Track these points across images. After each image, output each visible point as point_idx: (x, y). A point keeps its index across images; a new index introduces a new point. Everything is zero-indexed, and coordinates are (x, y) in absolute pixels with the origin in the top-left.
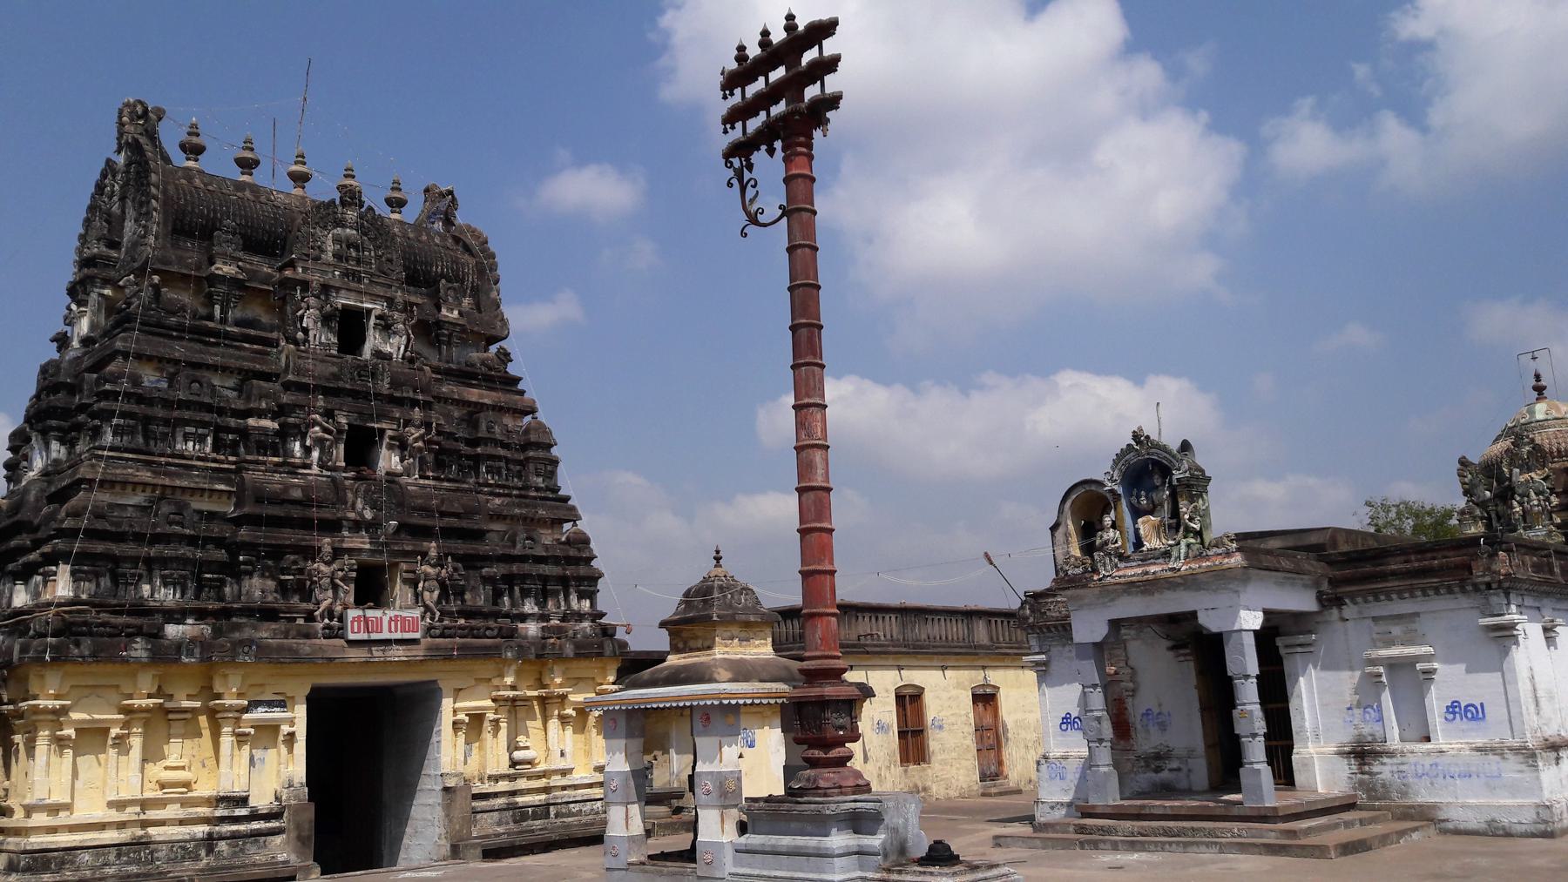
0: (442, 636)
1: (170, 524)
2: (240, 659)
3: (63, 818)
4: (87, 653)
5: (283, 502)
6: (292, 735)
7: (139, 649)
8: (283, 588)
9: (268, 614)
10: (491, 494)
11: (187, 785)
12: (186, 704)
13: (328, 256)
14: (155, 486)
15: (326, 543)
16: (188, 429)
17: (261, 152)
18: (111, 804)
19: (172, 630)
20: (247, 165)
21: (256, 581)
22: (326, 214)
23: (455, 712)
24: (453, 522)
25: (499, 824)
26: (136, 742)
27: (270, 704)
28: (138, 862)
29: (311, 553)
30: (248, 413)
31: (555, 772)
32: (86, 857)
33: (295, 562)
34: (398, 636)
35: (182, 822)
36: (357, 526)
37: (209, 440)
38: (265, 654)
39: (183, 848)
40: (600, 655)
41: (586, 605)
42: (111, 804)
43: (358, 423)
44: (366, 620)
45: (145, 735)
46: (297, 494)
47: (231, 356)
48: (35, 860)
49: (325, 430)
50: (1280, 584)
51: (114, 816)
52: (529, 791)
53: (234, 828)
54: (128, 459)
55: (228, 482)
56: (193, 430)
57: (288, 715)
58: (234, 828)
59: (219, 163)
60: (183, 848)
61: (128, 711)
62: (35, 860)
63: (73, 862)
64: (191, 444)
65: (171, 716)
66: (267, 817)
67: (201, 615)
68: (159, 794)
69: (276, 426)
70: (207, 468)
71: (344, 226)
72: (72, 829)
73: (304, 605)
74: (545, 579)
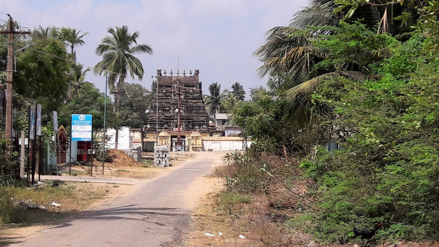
15: (172, 121)
20: (191, 74)
29: (171, 122)
36: (176, 119)
59: (168, 75)
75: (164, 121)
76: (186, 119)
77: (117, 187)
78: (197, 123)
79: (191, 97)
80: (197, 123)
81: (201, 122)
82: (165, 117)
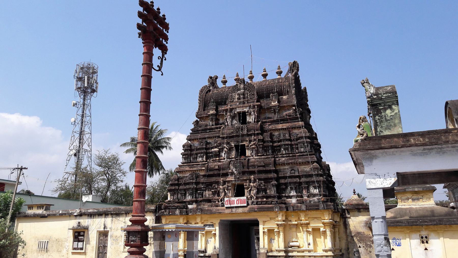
6: (215, 234)
7: (178, 212)
8: (214, 194)
9: (209, 201)
10: (282, 157)
13: (236, 100)
15: (221, 180)
18: (324, 250)
19: (190, 207)
20: (279, 73)
22: (235, 88)
23: (263, 228)
24: (261, 168)
27: (209, 225)
29: (218, 183)
31: (306, 250)
33: (214, 186)
34: (239, 205)
42: (324, 250)
46: (217, 167)
49: (227, 148)
50: (422, 154)
57: (214, 228)
59: (258, 79)
64: (200, 159)
67: (196, 202)
69: (218, 150)
71: (240, 90)
74: (300, 183)
76: (260, 172)
78: (289, 180)
79: (276, 117)
80: (289, 180)
81: (303, 180)
82: (208, 169)
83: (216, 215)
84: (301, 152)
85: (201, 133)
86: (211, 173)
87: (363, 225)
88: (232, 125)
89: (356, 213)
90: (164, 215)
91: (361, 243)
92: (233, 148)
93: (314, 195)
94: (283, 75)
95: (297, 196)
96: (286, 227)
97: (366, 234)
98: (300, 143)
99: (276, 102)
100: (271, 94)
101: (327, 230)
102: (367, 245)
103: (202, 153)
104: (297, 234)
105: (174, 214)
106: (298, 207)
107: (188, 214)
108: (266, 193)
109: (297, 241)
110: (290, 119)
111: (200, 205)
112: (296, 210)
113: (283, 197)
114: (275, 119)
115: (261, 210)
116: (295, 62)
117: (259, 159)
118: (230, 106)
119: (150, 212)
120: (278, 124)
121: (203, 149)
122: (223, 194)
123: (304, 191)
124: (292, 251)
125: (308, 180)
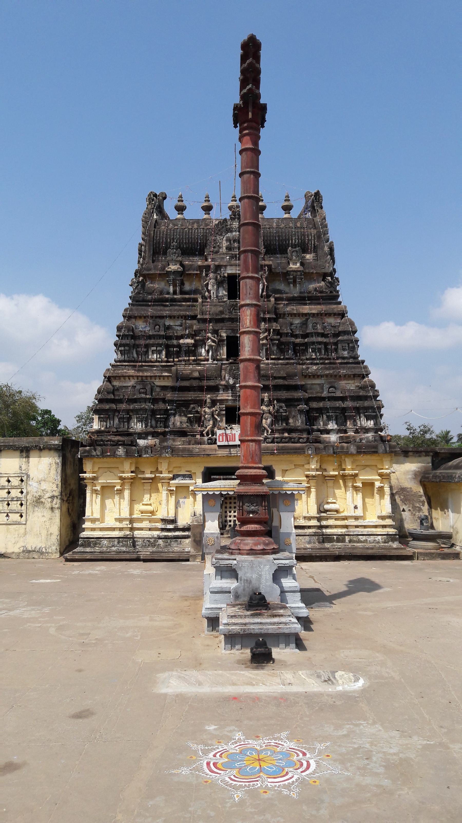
0: (273, 442)
1: (140, 393)
2: (164, 455)
3: (98, 525)
4: (99, 454)
5: (191, 379)
7: (121, 451)
8: (190, 421)
9: (182, 433)
10: (311, 364)
11: (152, 513)
12: (332, 473)
13: (224, 250)
14: (138, 377)
15: (208, 397)
16: (153, 348)
17: (213, 202)
18: (379, 517)
19: (141, 442)
20: (287, 209)
21: (177, 418)
22: (223, 226)
24: (281, 382)
25: (309, 543)
26: (127, 493)
27: (184, 476)
28: (126, 546)
29: (202, 403)
30: (182, 337)
31: (351, 517)
32: (105, 542)
33: (194, 408)
35: (150, 529)
36: (227, 388)
37: (164, 353)
38: (174, 452)
39: (149, 541)
40: (376, 452)
41: (371, 424)
42: (379, 517)
43: (232, 335)
44: (226, 435)
45: (131, 490)
46: (196, 374)
47: (175, 310)
48: (85, 542)
49: (214, 341)
51: (118, 525)
52: (336, 527)
53: (166, 534)
54: (125, 366)
55: (170, 371)
56: (155, 348)
58: (166, 534)
59: (194, 213)
60: (149, 541)
61: (121, 478)
62: (85, 542)
63: (100, 544)
64: (155, 355)
65: (327, 478)
66: (183, 530)
67: (155, 435)
68: (140, 516)
69: (193, 341)
70: (162, 366)
71: (231, 232)
72: (101, 529)
73: (200, 429)
74: (344, 410)
75: (169, 395)
76: (277, 388)
77: (301, 484)
78: (328, 404)
79: (295, 291)
80: (328, 404)
81: (349, 404)
82: (178, 377)
83: (198, 459)
84: (344, 358)
85: (153, 305)
86: (186, 384)
87: (410, 476)
88: (217, 296)
89: (402, 458)
90: (89, 456)
91: (405, 504)
92: (223, 341)
93: (367, 430)
94: (294, 214)
95: (339, 431)
96: (323, 482)
97: (415, 491)
98: (342, 341)
99: (298, 264)
100: (290, 248)
101: (386, 485)
102: (414, 507)
103: (160, 345)
104: (334, 491)
105: (114, 455)
106: (342, 448)
107: (140, 456)
108: (287, 423)
109: (334, 503)
110: (324, 298)
111: (166, 440)
112: (338, 453)
113: (313, 430)
114: (296, 295)
115: (283, 451)
116: (317, 194)
117: (274, 364)
118: (213, 260)
119: (50, 449)
120: (305, 304)
121: (160, 337)
122: (211, 422)
123: (348, 423)
124: (327, 519)
125: (357, 404)
